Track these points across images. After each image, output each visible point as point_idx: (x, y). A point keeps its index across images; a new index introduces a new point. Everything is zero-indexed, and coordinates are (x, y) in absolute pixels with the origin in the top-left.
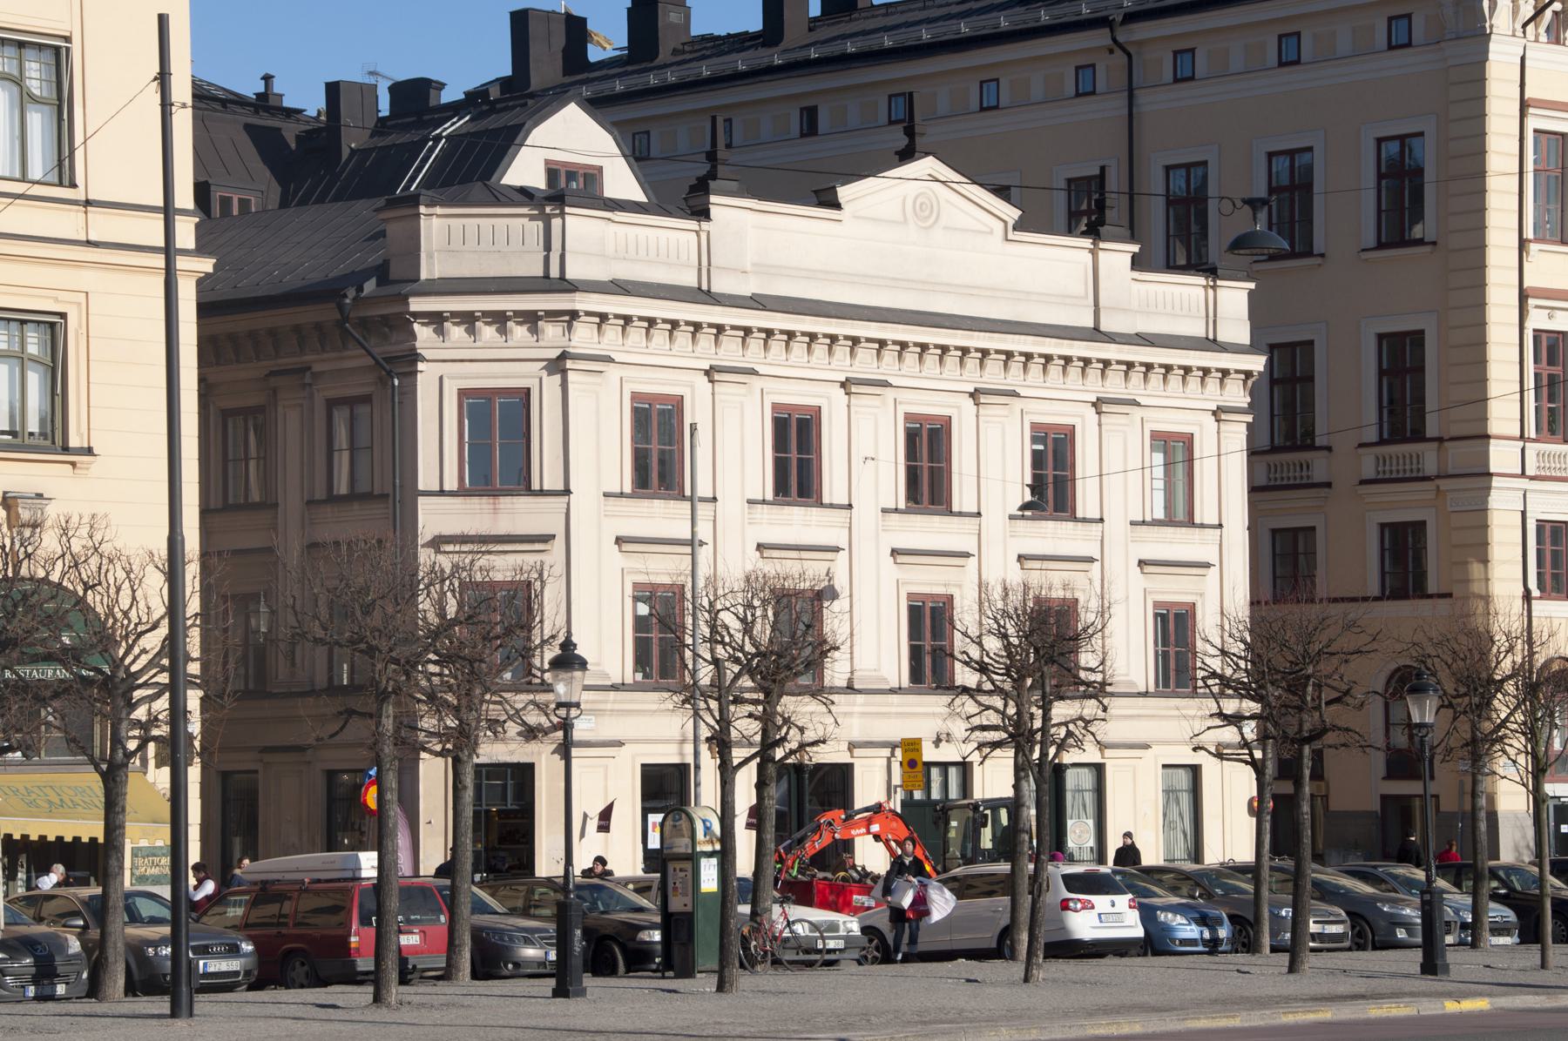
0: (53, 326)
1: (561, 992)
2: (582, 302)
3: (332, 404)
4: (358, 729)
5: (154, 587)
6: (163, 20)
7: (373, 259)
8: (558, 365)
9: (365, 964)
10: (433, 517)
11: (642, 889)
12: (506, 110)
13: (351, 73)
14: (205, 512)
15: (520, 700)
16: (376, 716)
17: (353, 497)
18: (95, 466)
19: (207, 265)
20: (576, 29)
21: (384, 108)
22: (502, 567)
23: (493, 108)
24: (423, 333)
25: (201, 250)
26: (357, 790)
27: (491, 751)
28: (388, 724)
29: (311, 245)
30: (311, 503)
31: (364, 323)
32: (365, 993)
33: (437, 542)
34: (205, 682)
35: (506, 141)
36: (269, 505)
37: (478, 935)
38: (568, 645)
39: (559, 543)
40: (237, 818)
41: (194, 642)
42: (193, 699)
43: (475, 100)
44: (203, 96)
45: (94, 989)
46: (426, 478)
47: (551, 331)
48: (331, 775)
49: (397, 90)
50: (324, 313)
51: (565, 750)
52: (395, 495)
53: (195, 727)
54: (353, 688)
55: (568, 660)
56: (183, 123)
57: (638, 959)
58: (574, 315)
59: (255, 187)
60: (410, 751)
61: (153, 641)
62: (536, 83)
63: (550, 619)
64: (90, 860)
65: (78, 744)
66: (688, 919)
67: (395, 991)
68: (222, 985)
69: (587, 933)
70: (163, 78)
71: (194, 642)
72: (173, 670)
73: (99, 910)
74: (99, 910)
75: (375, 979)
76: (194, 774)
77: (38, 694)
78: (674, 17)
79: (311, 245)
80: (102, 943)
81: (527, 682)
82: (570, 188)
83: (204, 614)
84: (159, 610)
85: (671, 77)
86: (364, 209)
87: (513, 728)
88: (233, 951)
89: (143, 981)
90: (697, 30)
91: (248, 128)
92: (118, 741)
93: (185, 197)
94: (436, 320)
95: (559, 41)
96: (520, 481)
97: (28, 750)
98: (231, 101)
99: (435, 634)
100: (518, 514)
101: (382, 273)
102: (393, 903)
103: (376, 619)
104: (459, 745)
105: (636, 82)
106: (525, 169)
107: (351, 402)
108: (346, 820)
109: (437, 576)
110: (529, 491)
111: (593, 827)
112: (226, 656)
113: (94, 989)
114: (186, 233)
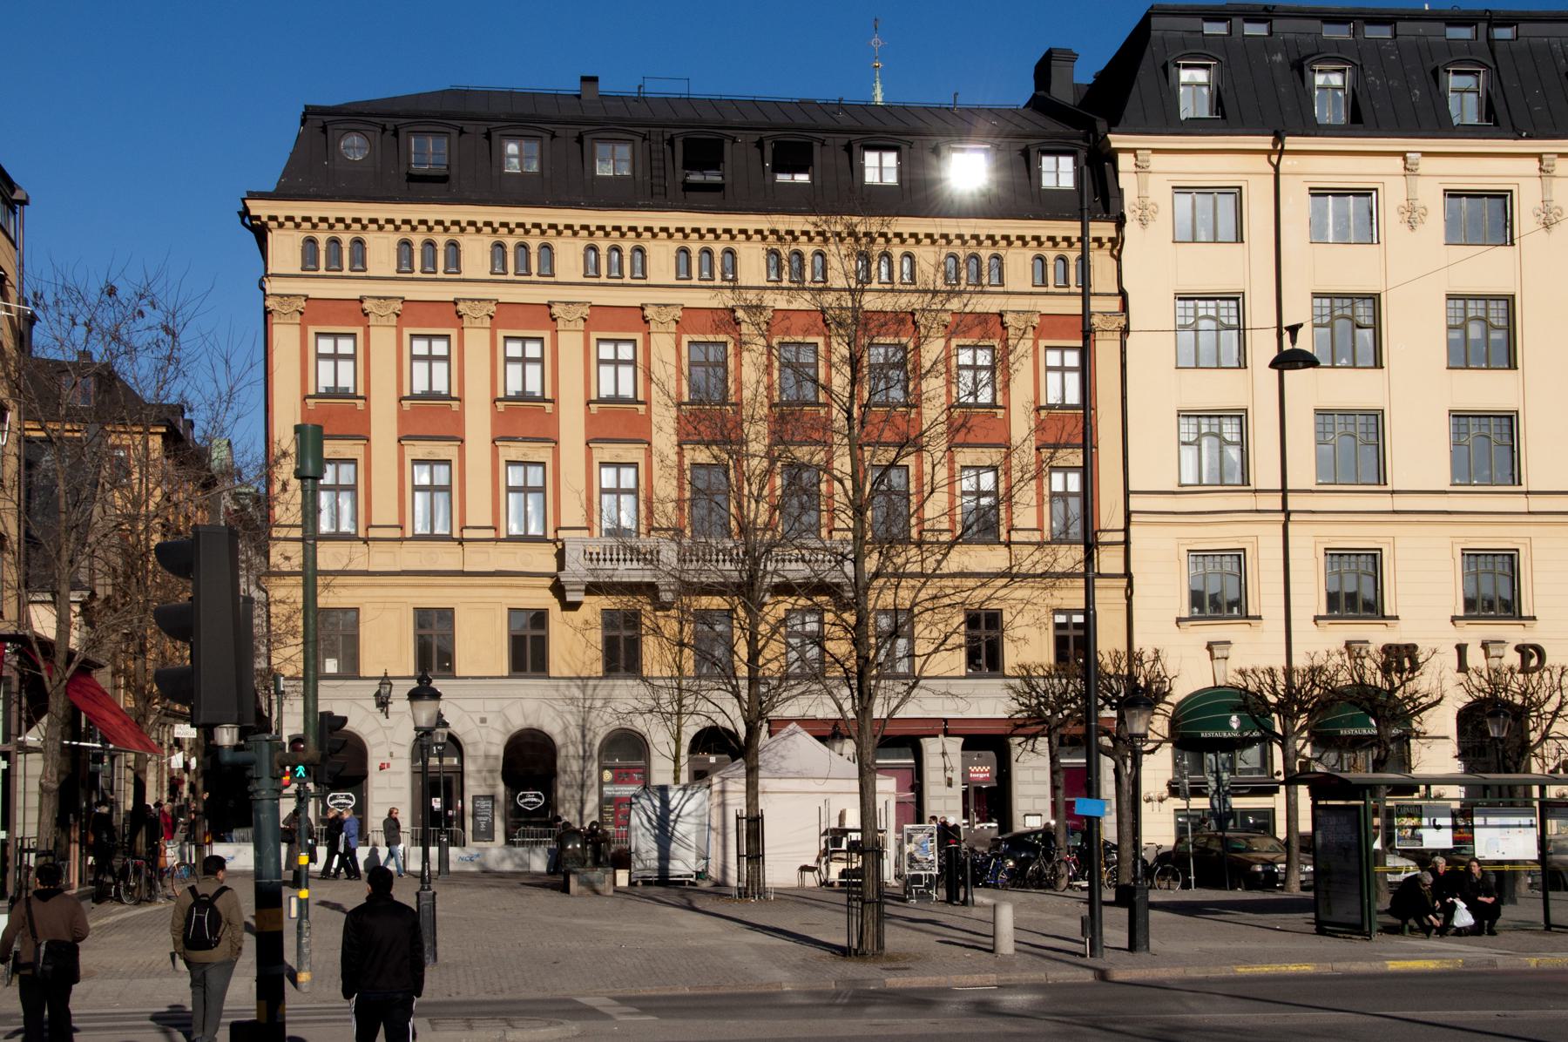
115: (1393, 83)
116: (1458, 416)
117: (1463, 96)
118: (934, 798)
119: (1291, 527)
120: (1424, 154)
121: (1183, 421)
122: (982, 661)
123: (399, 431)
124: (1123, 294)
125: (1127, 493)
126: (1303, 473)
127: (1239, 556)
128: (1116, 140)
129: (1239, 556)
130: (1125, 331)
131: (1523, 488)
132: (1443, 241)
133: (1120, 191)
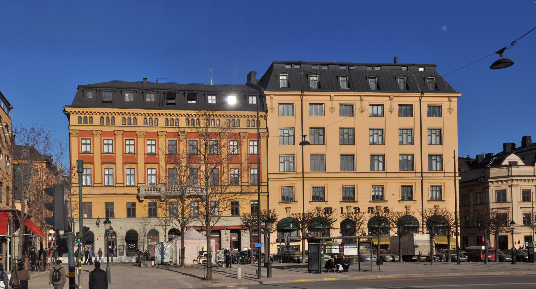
0: (440, 187)
1: (512, 263)
2: (514, 178)
3: (477, 193)
4: (481, 231)
5: (453, 216)
6: (454, 151)
7: (483, 175)
8: (511, 186)
9: (483, 259)
10: (491, 206)
11: (525, 251)
12: (502, 156)
13: (479, 153)
14: (460, 206)
15: (505, 228)
16: (484, 230)
17: (480, 204)
18: (446, 202)
19: (460, 178)
20: (513, 145)
21: (485, 157)
22: (502, 211)
23: (501, 155)
24: (490, 184)
25: (459, 176)
26: (481, 239)
27: (501, 234)
28: (486, 231)
29: (474, 174)
30: (474, 205)
31: (482, 183)
32: (484, 263)
33: (492, 209)
34: (460, 226)
35: (503, 159)
36: (468, 205)
37: (500, 257)
38: (513, 221)
39: (511, 209)
40: (465, 241)
41: (459, 222)
42: (459, 228)
43: (498, 155)
44: (460, 159)
45: (447, 261)
46: (491, 201)
47: (509, 182)
48: (478, 237)
49: (486, 155)
50: (476, 182)
51: (512, 234)
52: (486, 203)
53: (459, 231)
54: (481, 227)
55: (513, 223)
56: (457, 162)
57: (525, 260)
58: (513, 180)
59: (466, 168)
60: (489, 234)
61: (453, 222)
62: (507, 152)
63: (510, 217)
64: (447, 246)
65: (444, 233)
66: (532, 255)
67: (488, 263)
68: (464, 261)
69: (516, 256)
70: (454, 157)
71: (459, 222)
72: (456, 225)
73: (447, 252)
74: (447, 252)
75: (485, 261)
76: (459, 237)
77: (439, 228)
78: (529, 141)
79: (474, 174)
80: (448, 256)
81: (506, 225)
82: (513, 164)
83: (460, 218)
84: (454, 218)
85: (528, 149)
86: (482, 170)
87: (504, 231)
88: (465, 257)
89: (453, 260)
90: (532, 142)
91: (466, 162)
92: (449, 233)
93: (457, 170)
94: (492, 182)
95: (511, 146)
96: (505, 201)
97: (438, 234)
98: (463, 159)
99: (492, 220)
100: (504, 205)
101: (484, 177)
102: (487, 252)
103: (484, 218)
104: (496, 234)
105: (523, 150)
106: (506, 162)
107: (480, 193)
108: (479, 242)
109: (492, 213)
110: (506, 202)
111: (517, 241)
112: (362, 223)
113: (447, 261)
114: (457, 175)
116: (342, 156)
117: (343, 82)
120: (335, 95)
124: (267, 128)
125: (268, 174)
126: (307, 169)
128: (266, 93)
129: (293, 188)
130: (268, 137)
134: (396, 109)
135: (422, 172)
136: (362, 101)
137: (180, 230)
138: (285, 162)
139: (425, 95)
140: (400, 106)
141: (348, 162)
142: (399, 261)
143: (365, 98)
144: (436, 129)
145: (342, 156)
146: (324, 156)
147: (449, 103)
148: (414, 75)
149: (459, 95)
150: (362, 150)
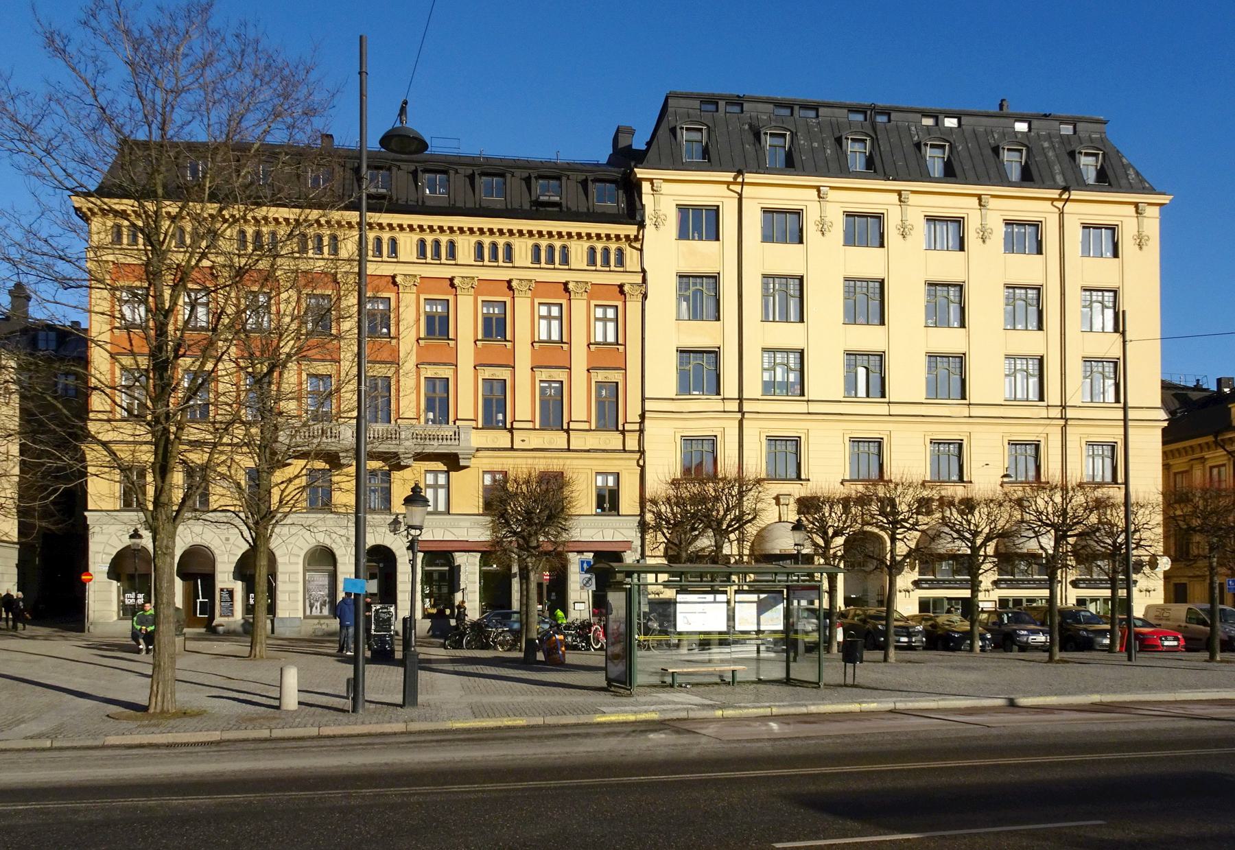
0: (797, 441)
3: (1211, 468)
115: (816, 145)
116: (932, 357)
117: (856, 152)
118: (284, 592)
119: (745, 422)
120: (831, 188)
121: (766, 355)
122: (607, 505)
123: (588, 363)
124: (644, 271)
125: (643, 399)
126: (753, 388)
127: (713, 441)
128: (640, 173)
129: (713, 441)
130: (645, 296)
131: (805, 398)
132: (842, 241)
133: (643, 206)
134: (1000, 230)
135: (741, 399)
136: (907, 206)
137: (151, 551)
138: (1019, 376)
139: (1075, 195)
140: (1008, 223)
141: (871, 371)
142: (1110, 649)
143: (993, 203)
144: (702, 277)
145: (932, 357)
146: (961, 358)
147: (1140, 221)
148: (1046, 145)
149: (1165, 199)
150: (908, 340)
